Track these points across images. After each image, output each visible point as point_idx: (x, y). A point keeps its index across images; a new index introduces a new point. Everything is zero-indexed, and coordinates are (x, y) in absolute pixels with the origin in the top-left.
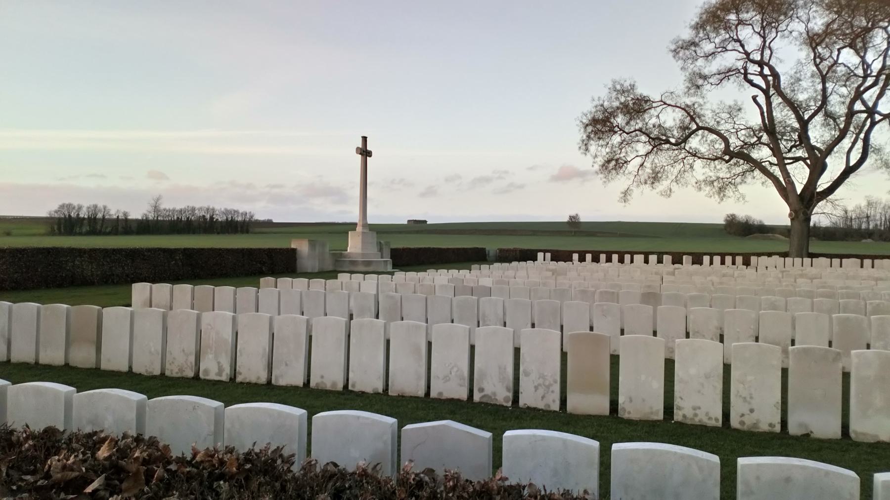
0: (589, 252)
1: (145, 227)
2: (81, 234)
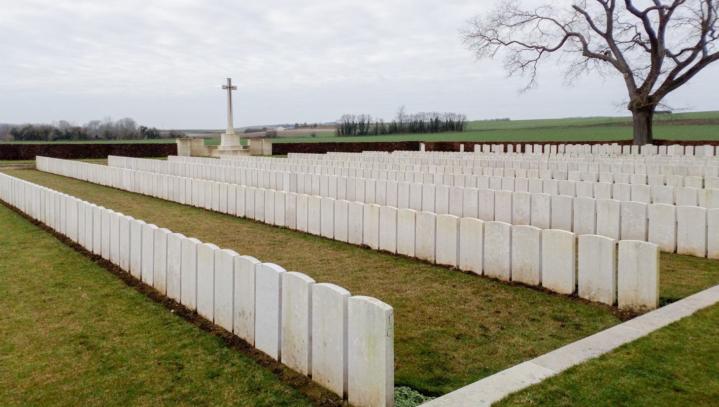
0: (518, 143)
1: (68, 136)
2: (355, 135)
